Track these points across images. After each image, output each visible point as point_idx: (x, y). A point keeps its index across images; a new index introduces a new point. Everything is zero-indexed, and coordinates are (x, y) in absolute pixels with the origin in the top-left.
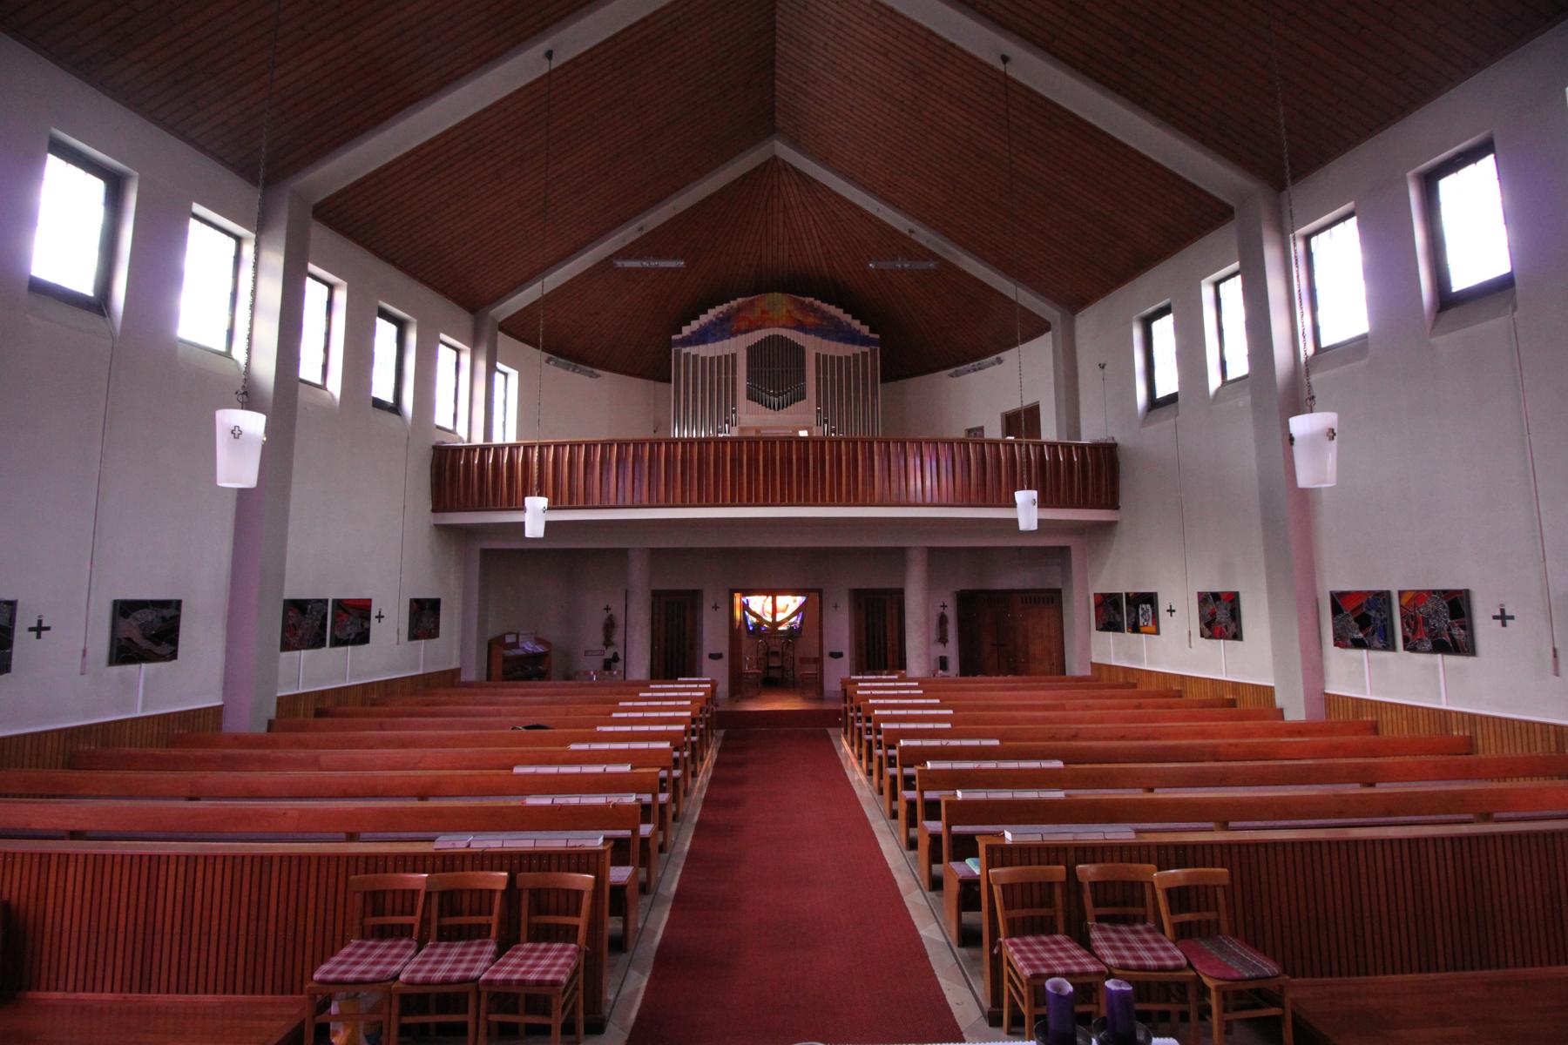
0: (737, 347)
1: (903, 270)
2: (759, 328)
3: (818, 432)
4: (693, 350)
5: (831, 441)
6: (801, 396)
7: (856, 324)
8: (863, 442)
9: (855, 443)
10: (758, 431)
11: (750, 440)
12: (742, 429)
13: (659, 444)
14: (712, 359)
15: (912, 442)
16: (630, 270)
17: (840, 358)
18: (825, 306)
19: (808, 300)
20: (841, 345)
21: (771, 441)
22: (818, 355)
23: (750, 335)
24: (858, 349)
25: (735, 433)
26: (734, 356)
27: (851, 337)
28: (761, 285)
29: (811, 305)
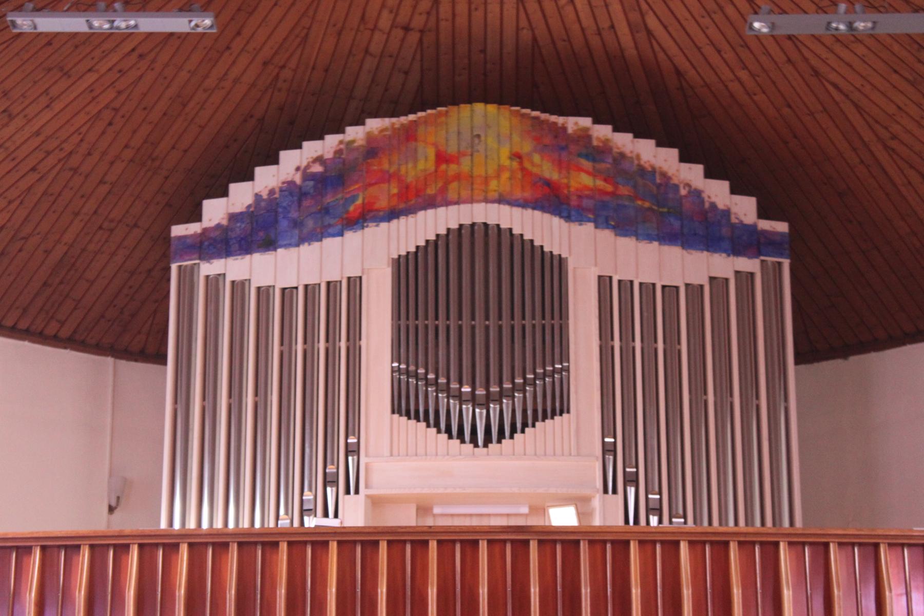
0: (367, 256)
1: (854, 37)
2: (431, 203)
3: (607, 514)
4: (234, 268)
5: (646, 544)
6: (556, 405)
7: (718, 192)
8: (746, 545)
9: (721, 547)
10: (423, 509)
11: (398, 540)
12: (376, 502)
13: (122, 549)
14: (287, 293)
15: (897, 544)
16: (52, 39)
17: (670, 291)
18: (624, 141)
19: (575, 123)
20: (674, 253)
21: (461, 543)
22: (604, 282)
23: (402, 224)
24: (724, 265)
25: (353, 514)
26: (355, 284)
27: (701, 229)
28: (440, 80)
29: (584, 136)
